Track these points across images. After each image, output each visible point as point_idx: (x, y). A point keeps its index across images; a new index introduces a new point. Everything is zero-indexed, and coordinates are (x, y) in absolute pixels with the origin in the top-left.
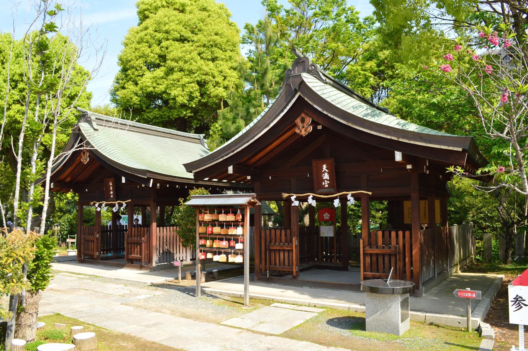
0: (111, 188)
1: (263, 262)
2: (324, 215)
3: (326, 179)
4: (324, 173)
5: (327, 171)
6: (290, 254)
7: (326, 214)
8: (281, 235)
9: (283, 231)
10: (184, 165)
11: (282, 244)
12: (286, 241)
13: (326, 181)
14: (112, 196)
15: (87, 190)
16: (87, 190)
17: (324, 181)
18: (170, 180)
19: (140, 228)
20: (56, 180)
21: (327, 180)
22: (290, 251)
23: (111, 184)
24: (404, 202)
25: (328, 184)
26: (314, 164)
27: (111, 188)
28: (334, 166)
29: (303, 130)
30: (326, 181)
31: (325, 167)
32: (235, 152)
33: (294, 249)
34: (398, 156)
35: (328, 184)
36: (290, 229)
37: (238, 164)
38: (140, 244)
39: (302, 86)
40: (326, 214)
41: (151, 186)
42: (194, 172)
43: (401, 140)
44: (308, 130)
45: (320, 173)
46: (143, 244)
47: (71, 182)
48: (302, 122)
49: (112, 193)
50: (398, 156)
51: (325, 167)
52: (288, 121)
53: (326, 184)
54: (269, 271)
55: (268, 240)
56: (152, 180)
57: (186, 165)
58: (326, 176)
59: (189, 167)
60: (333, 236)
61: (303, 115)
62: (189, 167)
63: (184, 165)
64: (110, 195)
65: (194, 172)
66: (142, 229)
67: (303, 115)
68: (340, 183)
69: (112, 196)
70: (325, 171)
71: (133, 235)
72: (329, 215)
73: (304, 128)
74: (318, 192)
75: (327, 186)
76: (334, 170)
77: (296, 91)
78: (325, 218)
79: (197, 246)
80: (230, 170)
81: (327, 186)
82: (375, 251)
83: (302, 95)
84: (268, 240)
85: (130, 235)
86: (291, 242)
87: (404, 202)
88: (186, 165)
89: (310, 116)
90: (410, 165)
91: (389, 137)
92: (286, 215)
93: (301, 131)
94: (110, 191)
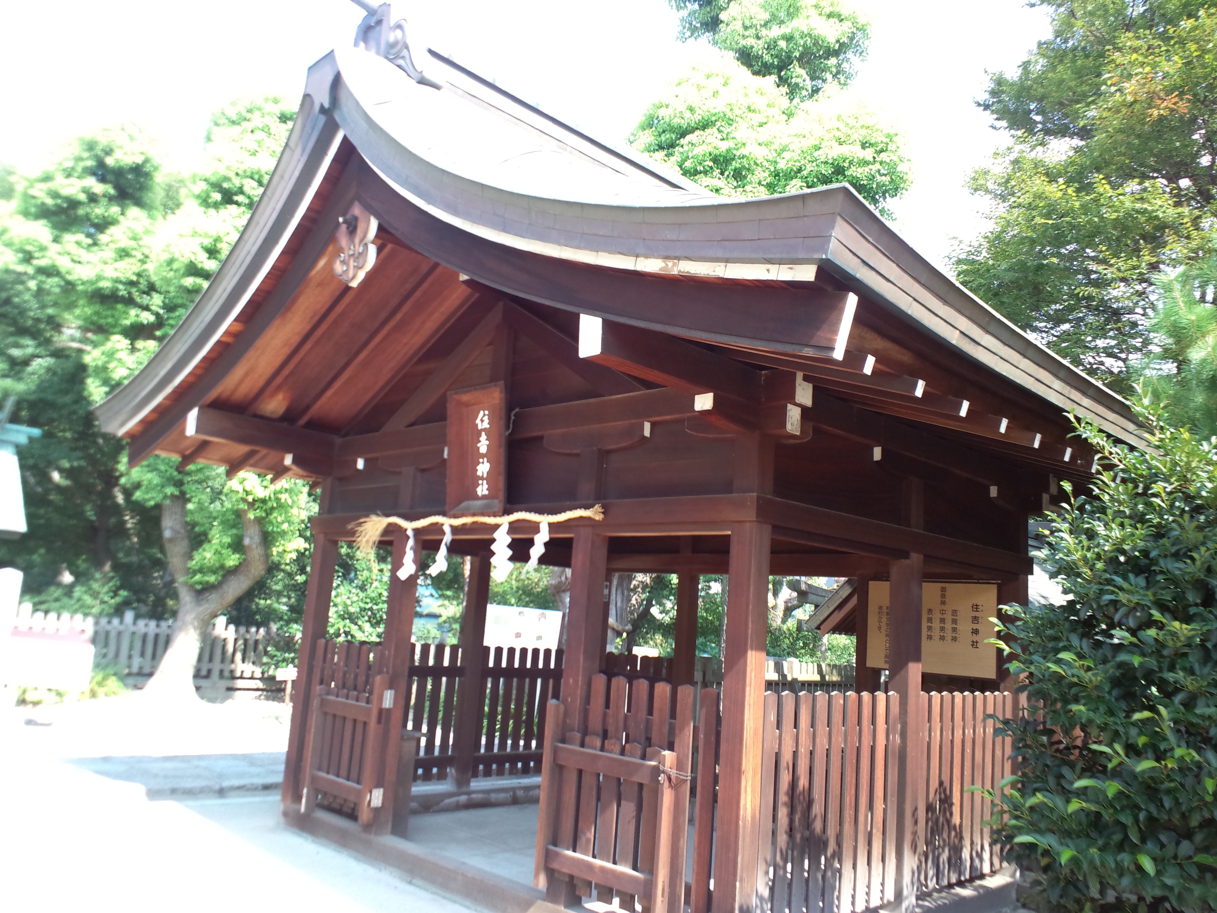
0: (483, 445)
8: (587, 699)
14: (482, 490)
15: (360, 464)
16: (360, 464)
19: (643, 684)
20: (213, 394)
23: (483, 421)
27: (483, 445)
38: (645, 799)
41: (502, 680)
46: (667, 797)
47: (289, 416)
49: (483, 468)
56: (852, 301)
64: (475, 480)
66: (663, 689)
69: (482, 490)
71: (595, 722)
85: (575, 720)
94: (476, 457)
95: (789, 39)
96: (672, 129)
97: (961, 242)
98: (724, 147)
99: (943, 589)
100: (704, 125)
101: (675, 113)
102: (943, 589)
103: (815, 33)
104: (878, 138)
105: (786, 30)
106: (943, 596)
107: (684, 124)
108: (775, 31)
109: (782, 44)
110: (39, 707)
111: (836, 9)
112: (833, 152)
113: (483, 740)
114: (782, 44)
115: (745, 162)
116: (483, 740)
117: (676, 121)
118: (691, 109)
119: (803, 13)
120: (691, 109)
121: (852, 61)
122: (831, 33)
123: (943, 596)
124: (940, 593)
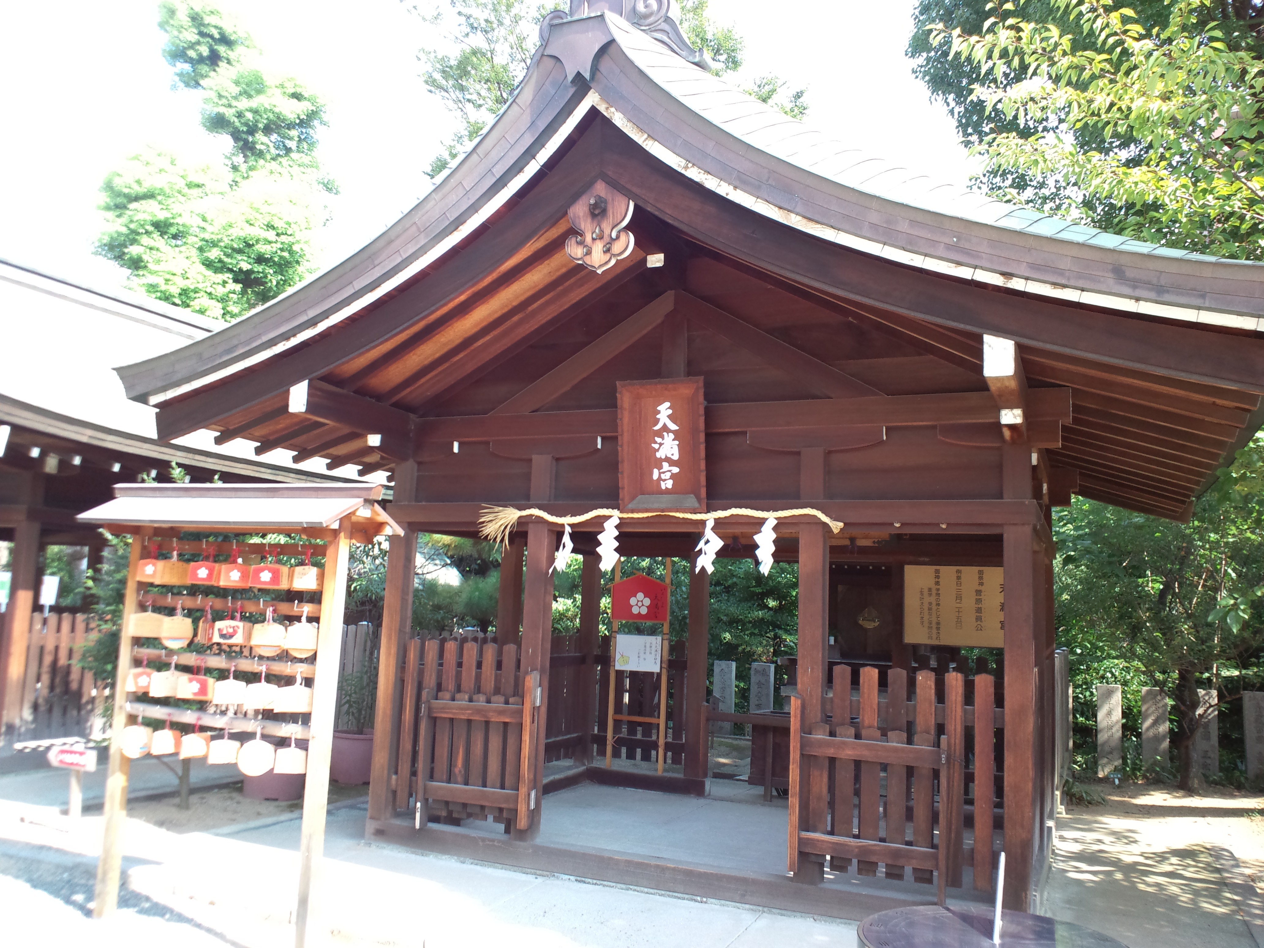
1: (405, 767)
2: (633, 601)
3: (667, 459)
4: (659, 433)
5: (673, 427)
6: (511, 741)
7: (640, 596)
8: (479, 665)
9: (490, 651)
10: (119, 370)
11: (482, 698)
12: (497, 691)
13: (666, 466)
17: (658, 464)
18: (84, 439)
21: (672, 463)
22: (510, 730)
24: (909, 570)
25: (673, 476)
26: (625, 397)
28: (702, 411)
29: (598, 248)
30: (666, 466)
31: (664, 411)
32: (322, 327)
33: (527, 720)
34: (999, 358)
35: (673, 476)
36: (517, 641)
37: (327, 378)
39: (606, 65)
40: (640, 596)
42: (155, 399)
43: (1017, 284)
44: (617, 248)
45: (646, 431)
48: (594, 216)
50: (999, 358)
51: (664, 411)
52: (541, 206)
53: (665, 477)
54: (425, 801)
55: (430, 680)
57: (128, 374)
58: (669, 447)
59: (138, 380)
60: (656, 669)
61: (600, 189)
62: (138, 380)
63: (119, 370)
65: (155, 399)
67: (600, 189)
68: (717, 472)
70: (665, 428)
72: (647, 602)
73: (605, 247)
74: (630, 506)
75: (669, 484)
76: (702, 426)
77: (582, 86)
78: (635, 610)
79: (119, 699)
80: (298, 398)
81: (669, 484)
82: (847, 748)
83: (602, 108)
84: (430, 680)
86: (518, 691)
87: (908, 569)
88: (128, 374)
89: (629, 195)
90: (1018, 412)
91: (965, 273)
92: (504, 581)
93: (589, 253)
95: (256, 112)
96: (125, 196)
97: (1032, 99)
98: (161, 216)
99: (981, 572)
100: (149, 196)
101: (126, 183)
102: (981, 572)
103: (277, 110)
104: (280, 224)
105: (255, 103)
106: (981, 578)
107: (133, 192)
108: (243, 104)
109: (249, 116)
110: (84, 756)
111: (299, 90)
112: (242, 231)
113: (953, 835)
114: (249, 116)
115: (181, 229)
116: (953, 835)
117: (126, 191)
118: (138, 182)
119: (269, 92)
120: (138, 182)
121: (318, 131)
122: (291, 110)
123: (981, 578)
124: (977, 576)
